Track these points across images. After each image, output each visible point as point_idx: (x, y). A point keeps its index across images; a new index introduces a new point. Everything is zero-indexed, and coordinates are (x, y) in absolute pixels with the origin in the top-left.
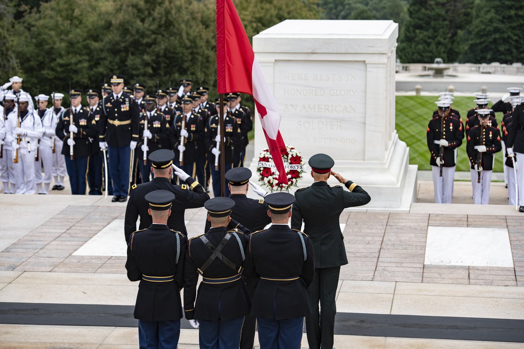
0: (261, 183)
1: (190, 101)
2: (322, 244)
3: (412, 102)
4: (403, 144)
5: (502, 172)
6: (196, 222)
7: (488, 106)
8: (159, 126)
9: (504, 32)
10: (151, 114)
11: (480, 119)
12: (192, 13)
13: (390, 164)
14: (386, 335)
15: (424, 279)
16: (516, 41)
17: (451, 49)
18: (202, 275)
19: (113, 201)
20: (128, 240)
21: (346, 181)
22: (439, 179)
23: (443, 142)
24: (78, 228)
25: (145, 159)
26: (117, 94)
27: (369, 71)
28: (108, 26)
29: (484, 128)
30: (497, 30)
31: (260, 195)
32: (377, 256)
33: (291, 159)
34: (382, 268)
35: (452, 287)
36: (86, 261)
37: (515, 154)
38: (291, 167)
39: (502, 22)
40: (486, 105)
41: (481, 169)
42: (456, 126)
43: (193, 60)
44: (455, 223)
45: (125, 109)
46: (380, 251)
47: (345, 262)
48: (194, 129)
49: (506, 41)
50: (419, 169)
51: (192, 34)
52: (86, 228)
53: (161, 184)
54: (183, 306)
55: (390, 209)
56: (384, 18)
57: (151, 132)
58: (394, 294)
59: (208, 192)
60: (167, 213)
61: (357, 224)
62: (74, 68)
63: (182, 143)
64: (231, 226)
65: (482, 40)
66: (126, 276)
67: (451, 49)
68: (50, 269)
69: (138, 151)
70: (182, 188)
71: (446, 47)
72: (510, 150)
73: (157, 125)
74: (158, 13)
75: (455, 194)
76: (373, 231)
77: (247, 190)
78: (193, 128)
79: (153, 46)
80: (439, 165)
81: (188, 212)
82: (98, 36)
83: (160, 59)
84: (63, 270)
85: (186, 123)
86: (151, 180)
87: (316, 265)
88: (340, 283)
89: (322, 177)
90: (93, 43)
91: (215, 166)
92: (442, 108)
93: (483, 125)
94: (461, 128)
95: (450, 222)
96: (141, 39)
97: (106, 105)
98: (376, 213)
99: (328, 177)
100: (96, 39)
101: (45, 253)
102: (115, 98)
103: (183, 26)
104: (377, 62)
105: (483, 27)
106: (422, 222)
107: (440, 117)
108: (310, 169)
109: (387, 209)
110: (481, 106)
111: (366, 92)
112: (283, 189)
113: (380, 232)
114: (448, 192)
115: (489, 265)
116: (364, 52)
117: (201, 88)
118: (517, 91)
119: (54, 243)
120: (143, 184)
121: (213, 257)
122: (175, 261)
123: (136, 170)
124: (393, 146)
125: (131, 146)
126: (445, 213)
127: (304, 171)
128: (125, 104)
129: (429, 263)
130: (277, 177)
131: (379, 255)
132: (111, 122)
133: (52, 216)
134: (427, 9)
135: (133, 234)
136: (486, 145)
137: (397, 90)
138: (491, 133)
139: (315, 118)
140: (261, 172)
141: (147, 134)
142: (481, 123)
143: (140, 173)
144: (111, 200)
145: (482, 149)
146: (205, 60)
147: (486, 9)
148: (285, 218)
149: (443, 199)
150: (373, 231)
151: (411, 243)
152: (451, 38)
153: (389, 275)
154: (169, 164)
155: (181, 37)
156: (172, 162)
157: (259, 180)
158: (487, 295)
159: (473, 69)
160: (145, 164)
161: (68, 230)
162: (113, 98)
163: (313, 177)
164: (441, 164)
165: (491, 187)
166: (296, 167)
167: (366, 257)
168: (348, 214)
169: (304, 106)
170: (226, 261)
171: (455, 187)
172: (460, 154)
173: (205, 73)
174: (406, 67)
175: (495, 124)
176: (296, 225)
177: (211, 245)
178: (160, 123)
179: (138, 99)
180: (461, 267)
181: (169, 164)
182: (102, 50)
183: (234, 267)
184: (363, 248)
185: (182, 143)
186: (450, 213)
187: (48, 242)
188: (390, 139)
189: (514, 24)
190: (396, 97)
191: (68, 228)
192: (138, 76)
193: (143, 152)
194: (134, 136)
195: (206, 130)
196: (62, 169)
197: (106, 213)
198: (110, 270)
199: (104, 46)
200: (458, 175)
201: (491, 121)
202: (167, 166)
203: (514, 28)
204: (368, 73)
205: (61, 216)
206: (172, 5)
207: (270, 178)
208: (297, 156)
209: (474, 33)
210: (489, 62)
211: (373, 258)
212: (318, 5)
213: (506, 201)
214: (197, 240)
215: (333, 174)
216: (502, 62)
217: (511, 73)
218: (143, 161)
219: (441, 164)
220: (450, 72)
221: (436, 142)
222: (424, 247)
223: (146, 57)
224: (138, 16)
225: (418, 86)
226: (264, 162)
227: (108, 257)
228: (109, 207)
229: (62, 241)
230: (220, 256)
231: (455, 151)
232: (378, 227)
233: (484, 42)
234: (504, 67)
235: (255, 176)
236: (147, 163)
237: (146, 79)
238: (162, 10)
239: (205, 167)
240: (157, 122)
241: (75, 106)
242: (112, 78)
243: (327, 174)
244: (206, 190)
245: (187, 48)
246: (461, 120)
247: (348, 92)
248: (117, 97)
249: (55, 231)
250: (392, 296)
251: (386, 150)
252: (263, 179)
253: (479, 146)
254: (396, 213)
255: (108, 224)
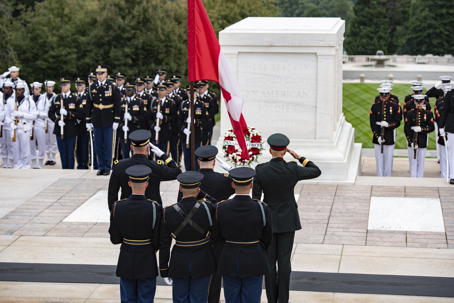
0: (226, 159)
1: (165, 88)
2: (279, 212)
3: (357, 89)
4: (349, 125)
5: (435, 149)
6: (170, 193)
7: (423, 92)
8: (138, 109)
9: (436, 28)
10: (131, 99)
11: (416, 103)
12: (166, 12)
13: (338, 142)
14: (334, 291)
15: (367, 242)
16: (447, 36)
17: (391, 43)
18: (175, 239)
19: (98, 175)
20: (111, 208)
21: (300, 157)
22: (380, 155)
23: (384, 124)
24: (68, 198)
25: (126, 138)
26: (102, 81)
27: (320, 62)
28: (94, 22)
29: (420, 111)
30: (430, 26)
31: (225, 169)
32: (327, 222)
33: (252, 138)
34: (331, 232)
35: (392, 249)
36: (75, 226)
37: (446, 134)
38: (252, 145)
39: (435, 19)
40: (421, 91)
41: (417, 147)
42: (395, 110)
43: (168, 52)
44: (394, 193)
45: (108, 95)
46: (329, 218)
47: (299, 228)
48: (168, 112)
49: (438, 35)
50: (363, 147)
51: (166, 29)
52: (74, 198)
53: (139, 160)
54: (158, 266)
55: (338, 182)
56: (333, 15)
57: (131, 114)
58: (341, 255)
59: (181, 167)
60: (145, 185)
61: (309, 195)
62: (64, 59)
63: (158, 124)
64: (200, 196)
65: (418, 35)
66: (109, 239)
67: (391, 43)
68: (43, 234)
69: (120, 131)
70: (158, 163)
71: (386, 41)
72: (442, 131)
73: (136, 108)
74: (137, 12)
75: (394, 169)
76: (323, 200)
77: (214, 165)
78: (167, 111)
79: (133, 40)
80: (381, 143)
81: (163, 184)
82: (85, 31)
83: (139, 51)
84: (55, 234)
85: (161, 106)
86: (131, 156)
87: (274, 230)
88: (294, 245)
89: (279, 154)
90: (80, 37)
91: (186, 144)
92: (383, 93)
93: (418, 108)
94: (399, 111)
95: (390, 193)
96: (122, 34)
97: (92, 92)
98: (326, 185)
99: (284, 154)
100: (83, 33)
101: (39, 220)
102: (100, 85)
103: (159, 23)
104: (326, 54)
105: (418, 23)
106: (366, 193)
107: (381, 102)
108: (269, 147)
109: (335, 181)
110: (417, 92)
111: (317, 80)
112: (245, 164)
113: (329, 201)
114: (388, 167)
115: (424, 230)
116: (315, 45)
117: (174, 77)
118: (448, 79)
119: (47, 211)
120: (124, 160)
121: (184, 223)
122: (152, 227)
123: (118, 147)
124: (341, 127)
125: (113, 127)
126: (385, 185)
127: (263, 148)
128: (108, 90)
129: (372, 229)
130: (240, 154)
131: (328, 222)
132: (96, 106)
133: (45, 188)
134: (370, 8)
135: (115, 203)
136: (421, 126)
137: (344, 78)
138: (425, 115)
139: (273, 102)
140: (227, 149)
141: (127, 116)
142: (417, 107)
143: (121, 151)
144: (96, 173)
145: (417, 129)
146: (177, 53)
147: (421, 8)
148: (247, 189)
149: (383, 173)
150: (323, 200)
151: (356, 211)
152: (391, 33)
153: (337, 238)
154: (146, 143)
155: (157, 33)
156: (149, 140)
157: (225, 157)
158: (422, 256)
159: (410, 60)
160: (126, 142)
161: (59, 199)
162: (98, 85)
163: (271, 153)
164: (382, 143)
165: (425, 162)
166: (256, 145)
167: (317, 223)
168: (302, 186)
169: (263, 92)
170: (196, 226)
171: (394, 162)
172: (399, 133)
173: (177, 63)
174: (352, 58)
175: (428, 107)
176: (257, 195)
177: (183, 213)
178: (138, 107)
179: (120, 86)
180: (400, 232)
181: (146, 143)
182: (88, 44)
183: (202, 232)
184: (315, 215)
185: (158, 124)
186: (390, 185)
187: (41, 210)
188: (338, 121)
189: (445, 21)
190: (343, 84)
191: (59, 198)
192: (119, 66)
193: (124, 132)
194: (116, 118)
195: (178, 113)
196: (54, 147)
197: (92, 185)
198: (96, 234)
199: (90, 40)
200: (397, 152)
201: (425, 105)
202: (145, 144)
203: (445, 25)
204: (319, 63)
205: (53, 188)
206: (149, 4)
207: (234, 154)
208: (257, 135)
209: (410, 28)
210: (424, 54)
211: (324, 224)
212: (276, 4)
213: (439, 174)
214: (171, 208)
215: (289, 151)
216: (435, 53)
217: (442, 64)
218: (124, 139)
219: (382, 143)
220: (390, 62)
221: (378, 123)
222: (367, 215)
223: (127, 50)
224: (119, 14)
225: (362, 75)
226: (228, 141)
227: (93, 223)
228: (94, 180)
229: (53, 209)
230: (191, 223)
231: (395, 131)
232: (328, 197)
233: (419, 36)
234: (436, 58)
235: (221, 152)
236: (127, 142)
237: (127, 68)
238: (141, 8)
239: (178, 145)
240: (136, 106)
241: (65, 92)
242: (97, 68)
243: (283, 151)
244: (179, 165)
245: (162, 42)
246: (399, 104)
247: (302, 80)
248: (102, 84)
249: (47, 200)
250: (340, 257)
251: (335, 130)
252: (227, 155)
253: (415, 127)
254: (343, 185)
255: (94, 194)
